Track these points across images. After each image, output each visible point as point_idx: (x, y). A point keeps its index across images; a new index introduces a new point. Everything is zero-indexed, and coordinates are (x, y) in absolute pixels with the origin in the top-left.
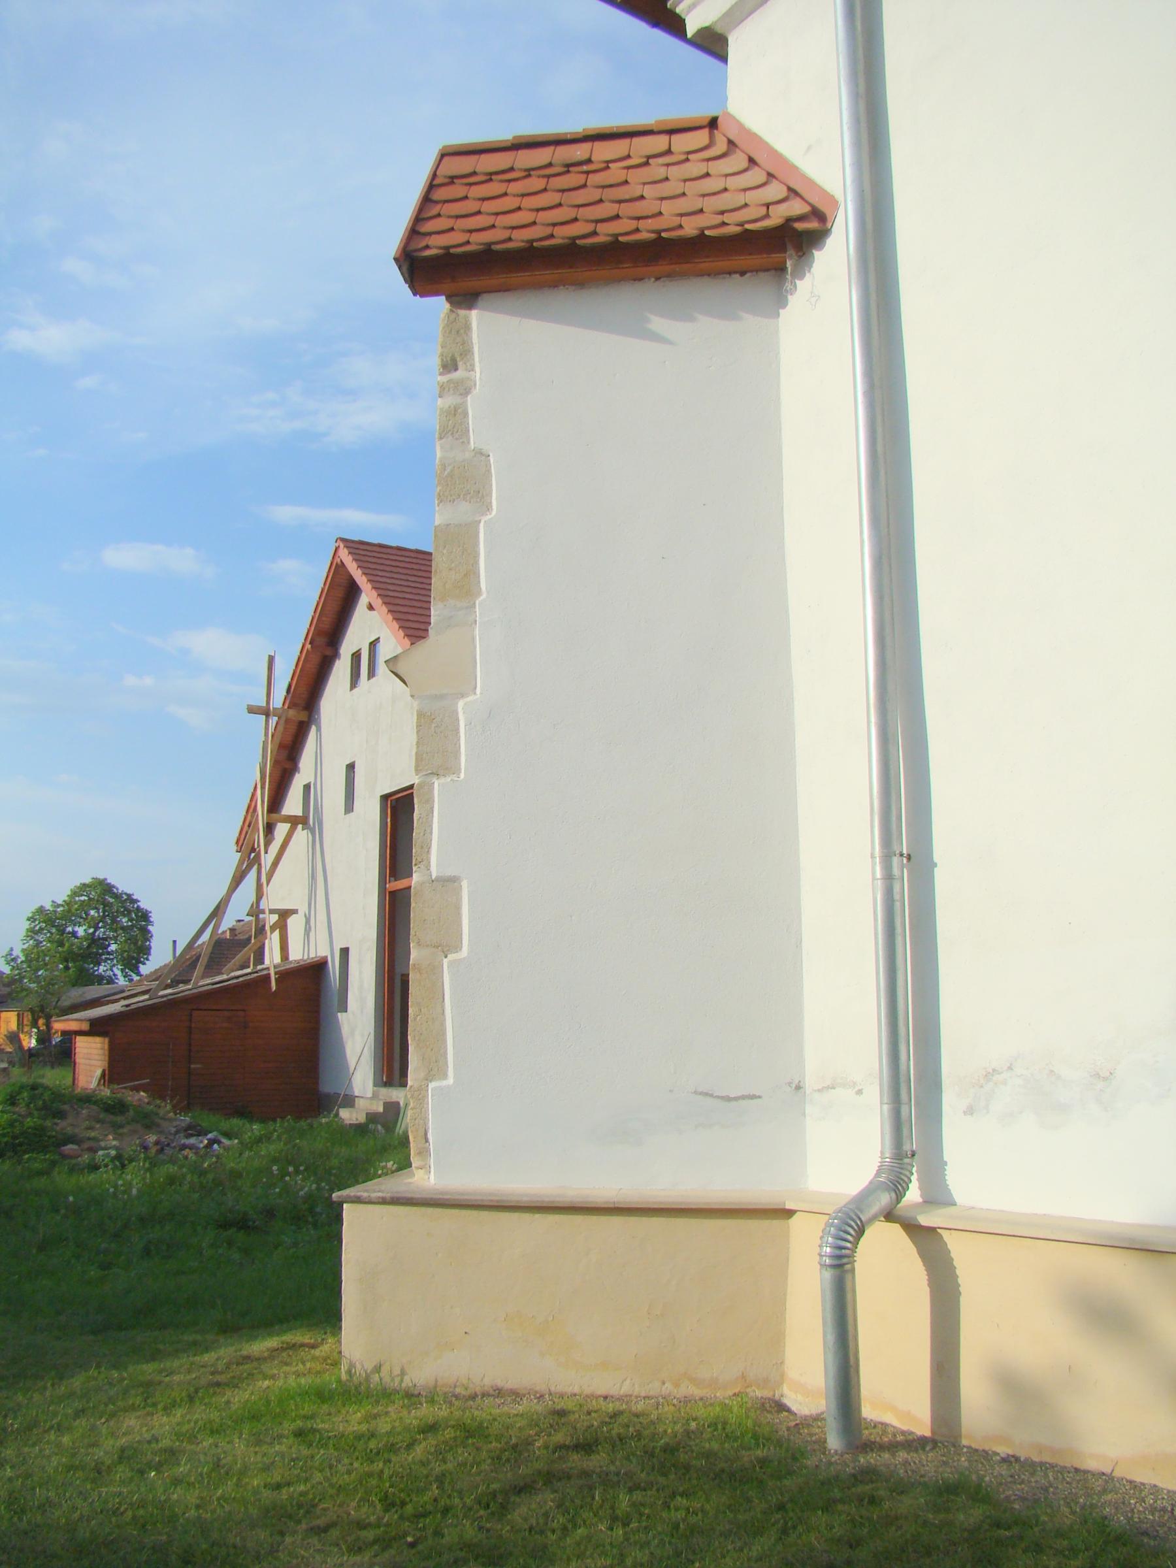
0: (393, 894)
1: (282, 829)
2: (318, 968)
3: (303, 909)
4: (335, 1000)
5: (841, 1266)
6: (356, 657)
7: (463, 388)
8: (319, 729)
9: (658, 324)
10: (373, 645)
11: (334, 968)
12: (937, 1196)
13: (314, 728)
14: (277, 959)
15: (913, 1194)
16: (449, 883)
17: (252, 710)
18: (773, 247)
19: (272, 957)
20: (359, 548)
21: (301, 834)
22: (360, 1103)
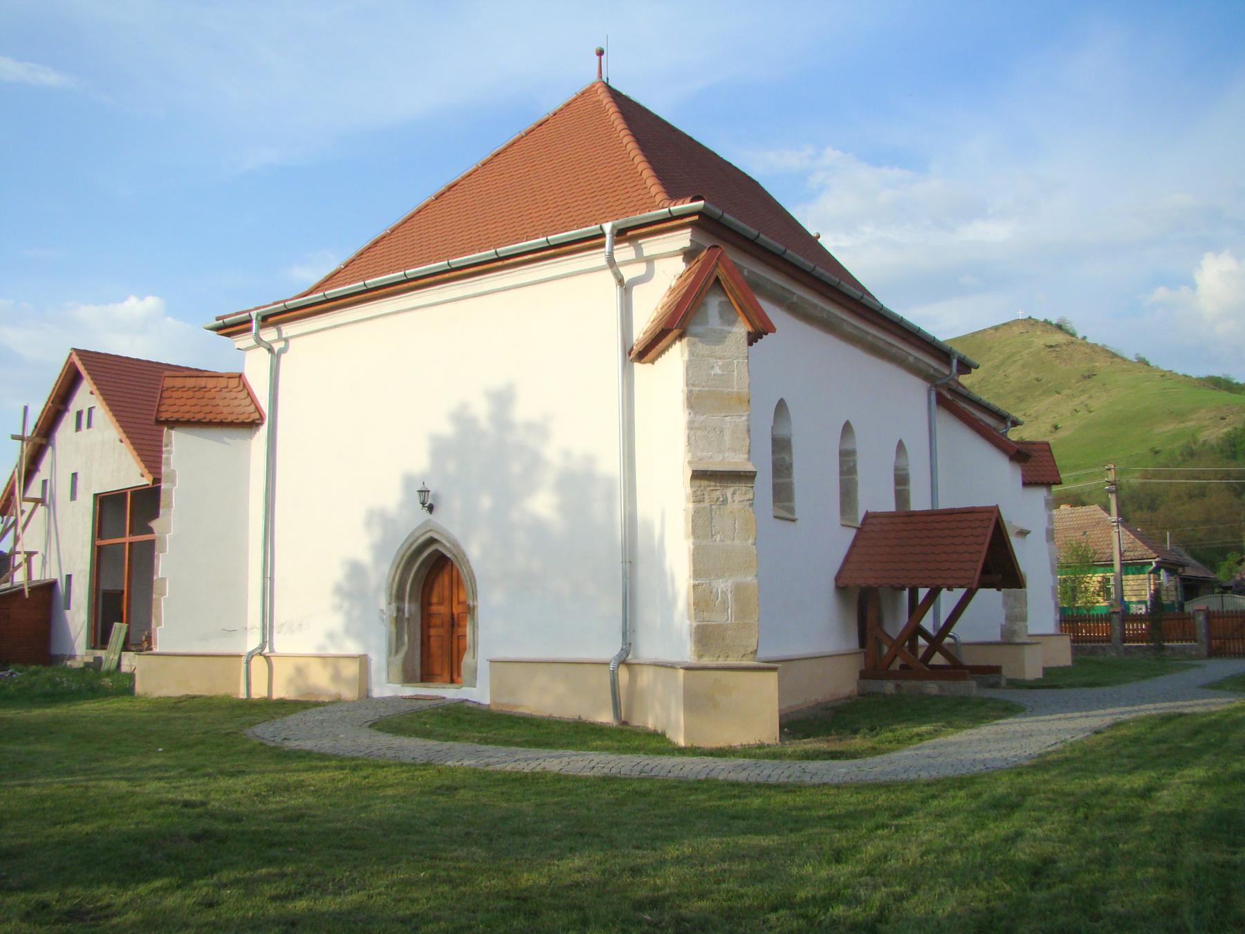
0: (99, 547)
2: (51, 586)
3: (41, 550)
4: (62, 603)
5: (248, 663)
6: (79, 414)
8: (54, 449)
9: (227, 440)
10: (90, 410)
11: (62, 586)
12: (272, 650)
13: (50, 449)
15: (267, 650)
16: (164, 579)
17: (14, 437)
18: (252, 425)
19: (19, 577)
20: (83, 354)
21: (41, 509)
22: (79, 659)
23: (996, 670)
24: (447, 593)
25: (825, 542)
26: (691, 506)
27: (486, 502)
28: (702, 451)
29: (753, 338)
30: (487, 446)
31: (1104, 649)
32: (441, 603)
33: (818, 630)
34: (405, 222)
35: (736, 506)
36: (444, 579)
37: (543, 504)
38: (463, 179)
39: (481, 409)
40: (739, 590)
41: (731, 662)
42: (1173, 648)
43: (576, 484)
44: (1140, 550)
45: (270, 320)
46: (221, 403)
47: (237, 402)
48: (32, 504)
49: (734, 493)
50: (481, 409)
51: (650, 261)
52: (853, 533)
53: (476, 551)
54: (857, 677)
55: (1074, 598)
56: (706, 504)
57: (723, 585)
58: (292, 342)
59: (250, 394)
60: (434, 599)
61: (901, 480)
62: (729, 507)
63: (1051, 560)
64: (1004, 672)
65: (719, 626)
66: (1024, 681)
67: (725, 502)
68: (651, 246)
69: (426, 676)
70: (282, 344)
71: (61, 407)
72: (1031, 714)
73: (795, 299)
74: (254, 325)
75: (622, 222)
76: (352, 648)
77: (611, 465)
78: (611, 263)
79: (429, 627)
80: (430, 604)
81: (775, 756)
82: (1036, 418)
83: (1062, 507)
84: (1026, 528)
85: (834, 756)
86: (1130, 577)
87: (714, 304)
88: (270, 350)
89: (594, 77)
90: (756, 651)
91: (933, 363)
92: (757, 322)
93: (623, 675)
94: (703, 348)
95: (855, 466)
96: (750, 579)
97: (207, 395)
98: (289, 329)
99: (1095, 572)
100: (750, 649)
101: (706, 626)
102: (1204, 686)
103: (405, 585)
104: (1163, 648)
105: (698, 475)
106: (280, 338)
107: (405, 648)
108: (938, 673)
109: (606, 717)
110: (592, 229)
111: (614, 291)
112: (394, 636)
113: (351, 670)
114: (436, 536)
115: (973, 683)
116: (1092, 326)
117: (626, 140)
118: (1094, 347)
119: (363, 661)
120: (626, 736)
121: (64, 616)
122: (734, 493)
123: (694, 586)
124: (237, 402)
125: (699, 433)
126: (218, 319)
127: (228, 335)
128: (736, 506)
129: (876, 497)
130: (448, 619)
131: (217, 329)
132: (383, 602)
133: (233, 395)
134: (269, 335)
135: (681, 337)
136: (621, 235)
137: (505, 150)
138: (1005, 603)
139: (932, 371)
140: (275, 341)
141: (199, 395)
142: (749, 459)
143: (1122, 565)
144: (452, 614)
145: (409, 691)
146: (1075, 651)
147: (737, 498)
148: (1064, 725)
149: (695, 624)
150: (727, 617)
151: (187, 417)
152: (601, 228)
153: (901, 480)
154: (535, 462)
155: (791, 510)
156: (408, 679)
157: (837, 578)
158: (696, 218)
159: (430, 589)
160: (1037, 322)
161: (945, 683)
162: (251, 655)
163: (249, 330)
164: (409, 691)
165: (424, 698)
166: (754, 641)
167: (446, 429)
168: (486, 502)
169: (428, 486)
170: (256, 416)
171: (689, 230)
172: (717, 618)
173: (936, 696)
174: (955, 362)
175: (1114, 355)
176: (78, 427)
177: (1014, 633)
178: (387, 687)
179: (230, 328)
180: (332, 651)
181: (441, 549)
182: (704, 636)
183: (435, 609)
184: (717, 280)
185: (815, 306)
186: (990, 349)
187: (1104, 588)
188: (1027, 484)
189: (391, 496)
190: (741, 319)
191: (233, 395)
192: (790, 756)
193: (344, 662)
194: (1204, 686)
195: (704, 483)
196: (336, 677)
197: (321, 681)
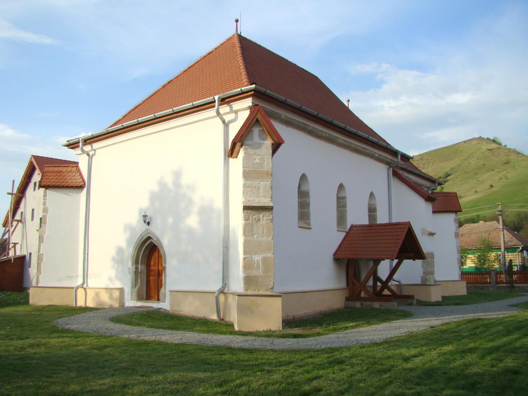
1: (15, 223)
2: (23, 258)
3: (20, 242)
6: (35, 183)
7: (46, 199)
8: (25, 199)
9: (71, 194)
12: (87, 286)
13: (24, 198)
14: (13, 255)
15: (85, 286)
16: (43, 254)
17: (9, 194)
18: (81, 187)
19: (11, 254)
20: (36, 158)
21: (20, 224)
23: (411, 297)
24: (157, 260)
25: (328, 238)
26: (243, 222)
27: (170, 220)
28: (250, 197)
29: (276, 147)
30: (171, 196)
31: (488, 287)
32: (154, 266)
33: (321, 280)
34: (149, 98)
35: (264, 222)
36: (156, 254)
37: (193, 221)
38: (175, 78)
39: (169, 180)
40: (265, 260)
41: (261, 292)
42: (519, 287)
43: (205, 212)
44: (515, 242)
45: (88, 141)
46: (68, 178)
47: (75, 178)
48: (16, 222)
49: (263, 216)
50: (169, 180)
51: (236, 112)
52: (344, 234)
53: (166, 243)
54: (344, 299)
55: (484, 264)
56: (250, 221)
57: (257, 258)
58: (97, 151)
59: (81, 174)
60: (152, 263)
61: (372, 210)
62: (261, 222)
63: (457, 246)
64: (416, 297)
65: (255, 276)
66: (430, 302)
67: (259, 220)
68: (237, 105)
69: (148, 298)
70: (93, 152)
71: (28, 181)
72: (417, 318)
73: (310, 128)
74: (81, 144)
75: (222, 95)
76: (118, 285)
77: (219, 204)
78: (218, 113)
79: (150, 276)
80: (150, 266)
81: (283, 336)
82: (483, 182)
83: (480, 222)
84: (434, 232)
85: (295, 336)
86: (510, 254)
87: (256, 131)
88: (88, 155)
89: (234, 32)
90: (273, 288)
91: (390, 157)
92: (276, 139)
93: (222, 298)
94: (251, 151)
95: (346, 203)
96: (270, 255)
97: (63, 174)
98: (96, 145)
99: (493, 252)
100: (270, 287)
101: (249, 276)
102: (509, 306)
103: (139, 257)
104: (514, 287)
105: (246, 208)
106: (92, 150)
107: (139, 285)
108: (387, 298)
109: (215, 317)
110: (210, 99)
111: (221, 126)
112: (134, 280)
113: (117, 294)
114: (151, 236)
115: (395, 304)
116: (509, 140)
117: (239, 59)
118: (509, 150)
119: (122, 290)
120: (223, 326)
121: (28, 271)
122: (263, 216)
123: (244, 258)
124: (75, 178)
125: (248, 189)
126: (67, 141)
127: (72, 148)
128: (264, 222)
129: (358, 216)
130: (157, 272)
131: (68, 146)
132: (129, 264)
133: (73, 174)
134: (87, 148)
135: (242, 146)
136: (223, 101)
137: (193, 65)
138: (423, 266)
139: (389, 160)
140: (90, 151)
141: (59, 174)
142: (271, 201)
143: (505, 249)
144: (159, 270)
145: (139, 304)
146: (468, 288)
147: (265, 218)
148: (423, 323)
149: (244, 275)
150: (259, 272)
151: (53, 184)
152: (214, 98)
153: (372, 210)
154: (190, 202)
155: (309, 224)
156: (140, 298)
157: (335, 255)
158: (253, 92)
159: (149, 257)
160: (483, 139)
161: (382, 303)
162: (78, 288)
163: (78, 146)
164: (139, 304)
165: (146, 307)
166: (272, 283)
167: (156, 188)
168: (170, 220)
169: (147, 214)
170: (83, 183)
171: (251, 98)
172: (255, 273)
173: (377, 309)
174: (399, 156)
175: (519, 153)
176: (35, 190)
177: (427, 280)
178: (131, 302)
179: (73, 145)
180: (112, 286)
181: (153, 241)
182: (248, 280)
183: (152, 268)
184: (257, 120)
185: (322, 132)
186: (462, 151)
187: (497, 258)
188: (434, 212)
189: (134, 219)
190: (269, 137)
191: (73, 174)
192: (275, 336)
193: (114, 291)
194: (509, 306)
195: (249, 212)
196: (111, 297)
197: (105, 298)
